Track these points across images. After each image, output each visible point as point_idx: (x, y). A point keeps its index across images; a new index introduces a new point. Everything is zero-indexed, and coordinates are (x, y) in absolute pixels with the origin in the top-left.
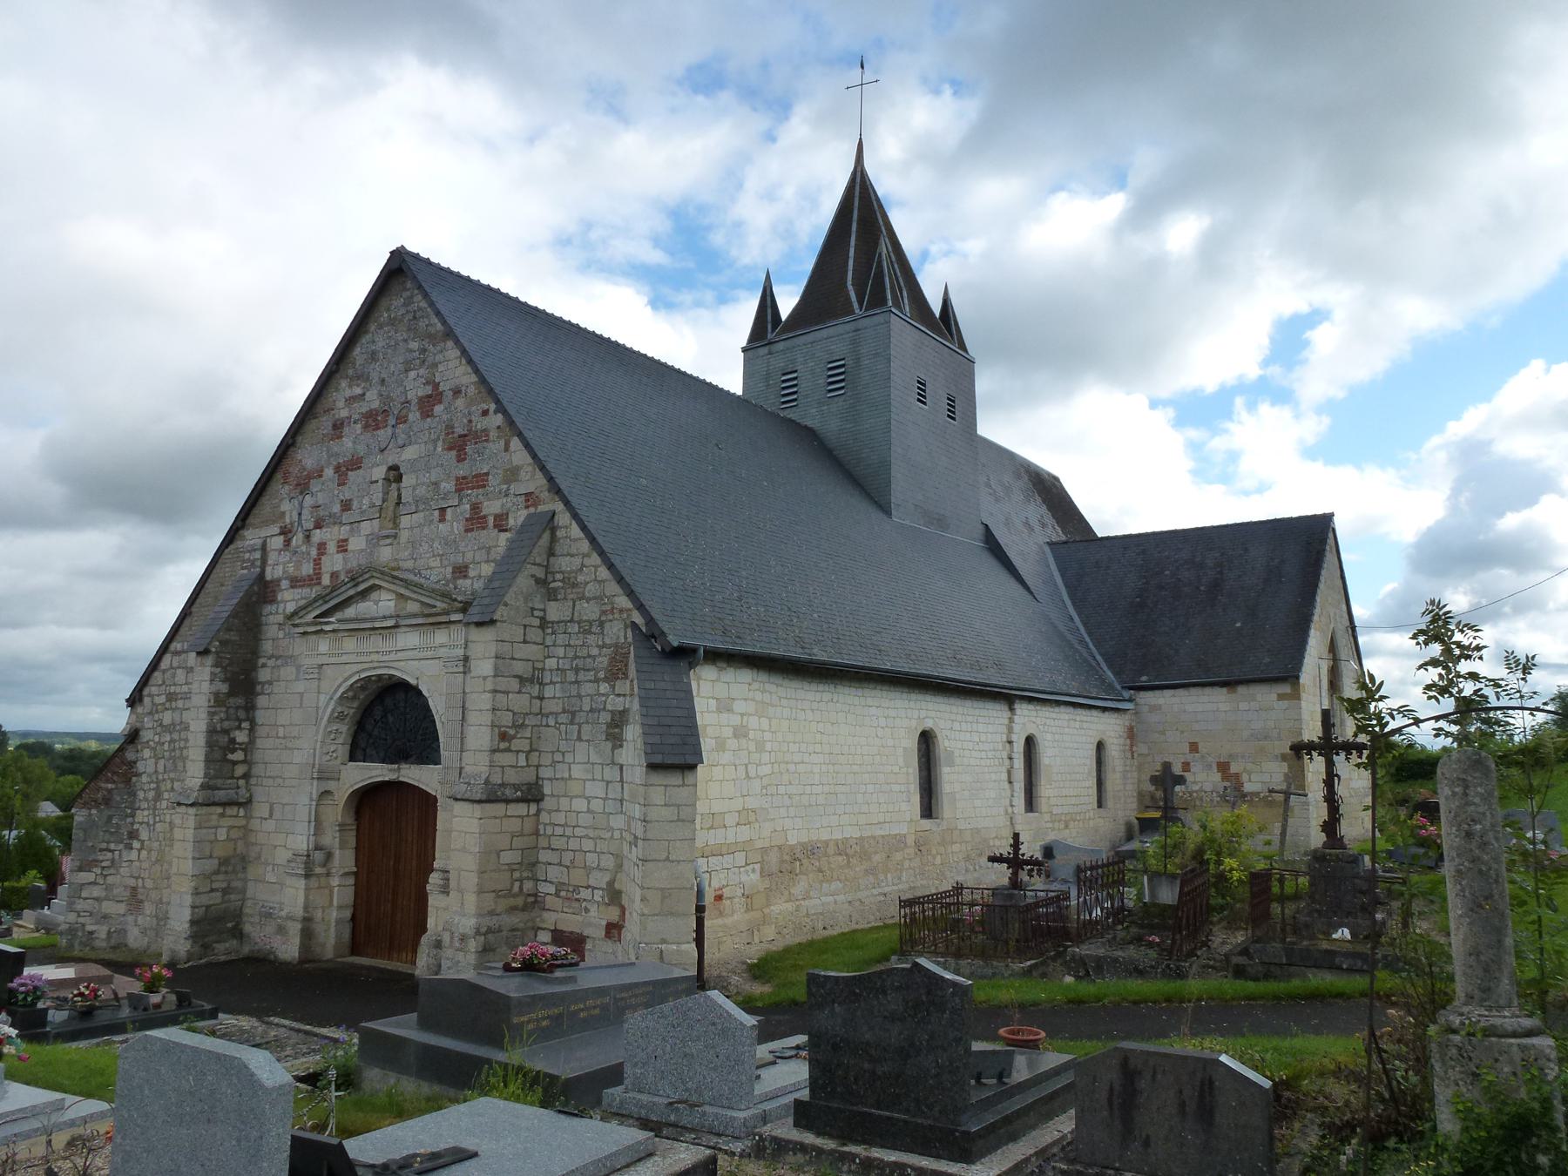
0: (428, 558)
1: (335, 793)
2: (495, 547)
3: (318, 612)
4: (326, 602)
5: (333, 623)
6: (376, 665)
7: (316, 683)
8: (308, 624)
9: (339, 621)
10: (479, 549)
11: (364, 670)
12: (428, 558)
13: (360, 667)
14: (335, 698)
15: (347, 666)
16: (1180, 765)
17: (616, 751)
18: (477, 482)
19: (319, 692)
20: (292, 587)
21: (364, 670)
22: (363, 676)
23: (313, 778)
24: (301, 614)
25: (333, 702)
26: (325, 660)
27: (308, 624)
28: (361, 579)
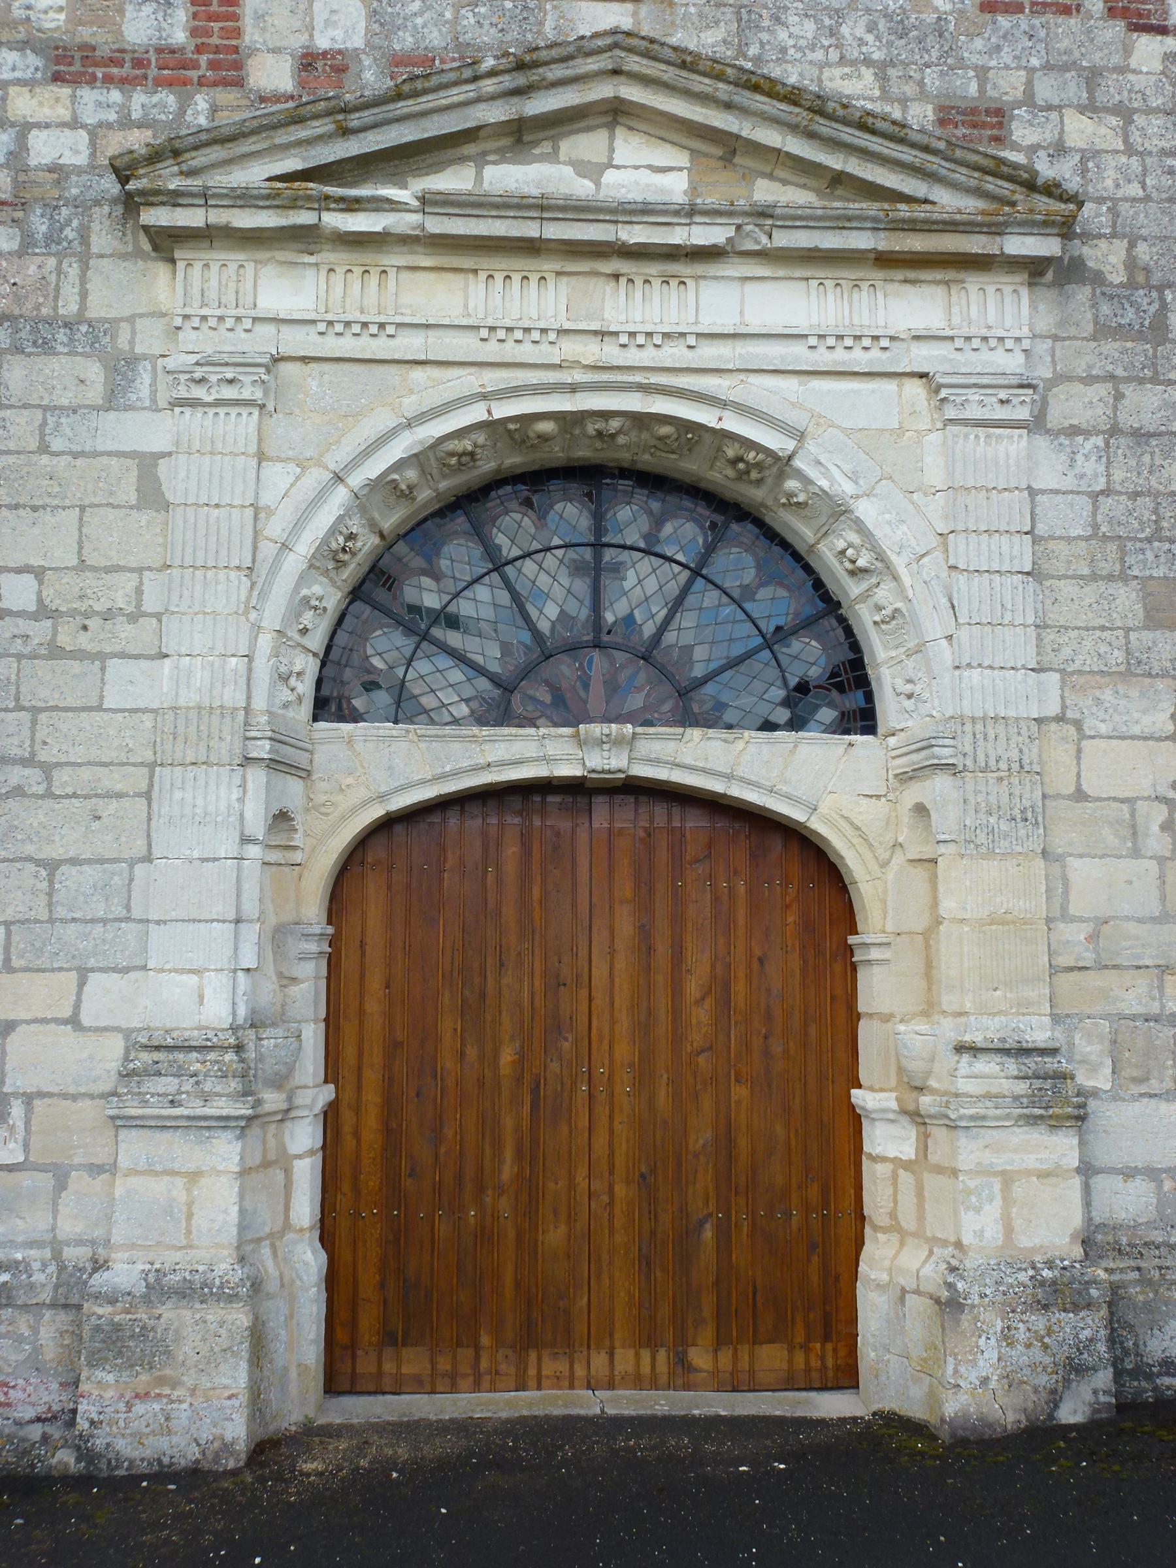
0: (823, 65)
1: (298, 821)
2: (1123, 70)
3: (292, 163)
4: (345, 132)
5: (391, 205)
6: (578, 376)
7: (249, 421)
8: (243, 198)
9: (427, 202)
10: (1047, 67)
11: (515, 392)
12: (823, 65)
13: (492, 379)
14: (356, 480)
15: (418, 375)
16: (994, 1203)
17: (1155, 862)
18: (213, 65)
19: (261, 457)
20: (57, 78)
21: (515, 392)
22: (503, 410)
23: (247, 761)
24: (199, 159)
25: (340, 497)
26: (296, 341)
27: (243, 198)
28: (557, 72)
